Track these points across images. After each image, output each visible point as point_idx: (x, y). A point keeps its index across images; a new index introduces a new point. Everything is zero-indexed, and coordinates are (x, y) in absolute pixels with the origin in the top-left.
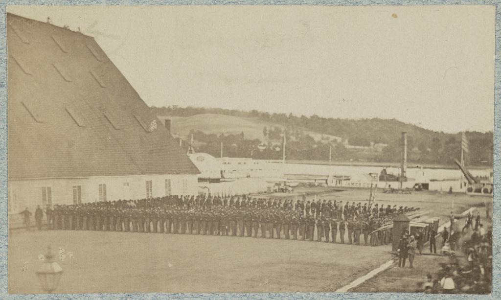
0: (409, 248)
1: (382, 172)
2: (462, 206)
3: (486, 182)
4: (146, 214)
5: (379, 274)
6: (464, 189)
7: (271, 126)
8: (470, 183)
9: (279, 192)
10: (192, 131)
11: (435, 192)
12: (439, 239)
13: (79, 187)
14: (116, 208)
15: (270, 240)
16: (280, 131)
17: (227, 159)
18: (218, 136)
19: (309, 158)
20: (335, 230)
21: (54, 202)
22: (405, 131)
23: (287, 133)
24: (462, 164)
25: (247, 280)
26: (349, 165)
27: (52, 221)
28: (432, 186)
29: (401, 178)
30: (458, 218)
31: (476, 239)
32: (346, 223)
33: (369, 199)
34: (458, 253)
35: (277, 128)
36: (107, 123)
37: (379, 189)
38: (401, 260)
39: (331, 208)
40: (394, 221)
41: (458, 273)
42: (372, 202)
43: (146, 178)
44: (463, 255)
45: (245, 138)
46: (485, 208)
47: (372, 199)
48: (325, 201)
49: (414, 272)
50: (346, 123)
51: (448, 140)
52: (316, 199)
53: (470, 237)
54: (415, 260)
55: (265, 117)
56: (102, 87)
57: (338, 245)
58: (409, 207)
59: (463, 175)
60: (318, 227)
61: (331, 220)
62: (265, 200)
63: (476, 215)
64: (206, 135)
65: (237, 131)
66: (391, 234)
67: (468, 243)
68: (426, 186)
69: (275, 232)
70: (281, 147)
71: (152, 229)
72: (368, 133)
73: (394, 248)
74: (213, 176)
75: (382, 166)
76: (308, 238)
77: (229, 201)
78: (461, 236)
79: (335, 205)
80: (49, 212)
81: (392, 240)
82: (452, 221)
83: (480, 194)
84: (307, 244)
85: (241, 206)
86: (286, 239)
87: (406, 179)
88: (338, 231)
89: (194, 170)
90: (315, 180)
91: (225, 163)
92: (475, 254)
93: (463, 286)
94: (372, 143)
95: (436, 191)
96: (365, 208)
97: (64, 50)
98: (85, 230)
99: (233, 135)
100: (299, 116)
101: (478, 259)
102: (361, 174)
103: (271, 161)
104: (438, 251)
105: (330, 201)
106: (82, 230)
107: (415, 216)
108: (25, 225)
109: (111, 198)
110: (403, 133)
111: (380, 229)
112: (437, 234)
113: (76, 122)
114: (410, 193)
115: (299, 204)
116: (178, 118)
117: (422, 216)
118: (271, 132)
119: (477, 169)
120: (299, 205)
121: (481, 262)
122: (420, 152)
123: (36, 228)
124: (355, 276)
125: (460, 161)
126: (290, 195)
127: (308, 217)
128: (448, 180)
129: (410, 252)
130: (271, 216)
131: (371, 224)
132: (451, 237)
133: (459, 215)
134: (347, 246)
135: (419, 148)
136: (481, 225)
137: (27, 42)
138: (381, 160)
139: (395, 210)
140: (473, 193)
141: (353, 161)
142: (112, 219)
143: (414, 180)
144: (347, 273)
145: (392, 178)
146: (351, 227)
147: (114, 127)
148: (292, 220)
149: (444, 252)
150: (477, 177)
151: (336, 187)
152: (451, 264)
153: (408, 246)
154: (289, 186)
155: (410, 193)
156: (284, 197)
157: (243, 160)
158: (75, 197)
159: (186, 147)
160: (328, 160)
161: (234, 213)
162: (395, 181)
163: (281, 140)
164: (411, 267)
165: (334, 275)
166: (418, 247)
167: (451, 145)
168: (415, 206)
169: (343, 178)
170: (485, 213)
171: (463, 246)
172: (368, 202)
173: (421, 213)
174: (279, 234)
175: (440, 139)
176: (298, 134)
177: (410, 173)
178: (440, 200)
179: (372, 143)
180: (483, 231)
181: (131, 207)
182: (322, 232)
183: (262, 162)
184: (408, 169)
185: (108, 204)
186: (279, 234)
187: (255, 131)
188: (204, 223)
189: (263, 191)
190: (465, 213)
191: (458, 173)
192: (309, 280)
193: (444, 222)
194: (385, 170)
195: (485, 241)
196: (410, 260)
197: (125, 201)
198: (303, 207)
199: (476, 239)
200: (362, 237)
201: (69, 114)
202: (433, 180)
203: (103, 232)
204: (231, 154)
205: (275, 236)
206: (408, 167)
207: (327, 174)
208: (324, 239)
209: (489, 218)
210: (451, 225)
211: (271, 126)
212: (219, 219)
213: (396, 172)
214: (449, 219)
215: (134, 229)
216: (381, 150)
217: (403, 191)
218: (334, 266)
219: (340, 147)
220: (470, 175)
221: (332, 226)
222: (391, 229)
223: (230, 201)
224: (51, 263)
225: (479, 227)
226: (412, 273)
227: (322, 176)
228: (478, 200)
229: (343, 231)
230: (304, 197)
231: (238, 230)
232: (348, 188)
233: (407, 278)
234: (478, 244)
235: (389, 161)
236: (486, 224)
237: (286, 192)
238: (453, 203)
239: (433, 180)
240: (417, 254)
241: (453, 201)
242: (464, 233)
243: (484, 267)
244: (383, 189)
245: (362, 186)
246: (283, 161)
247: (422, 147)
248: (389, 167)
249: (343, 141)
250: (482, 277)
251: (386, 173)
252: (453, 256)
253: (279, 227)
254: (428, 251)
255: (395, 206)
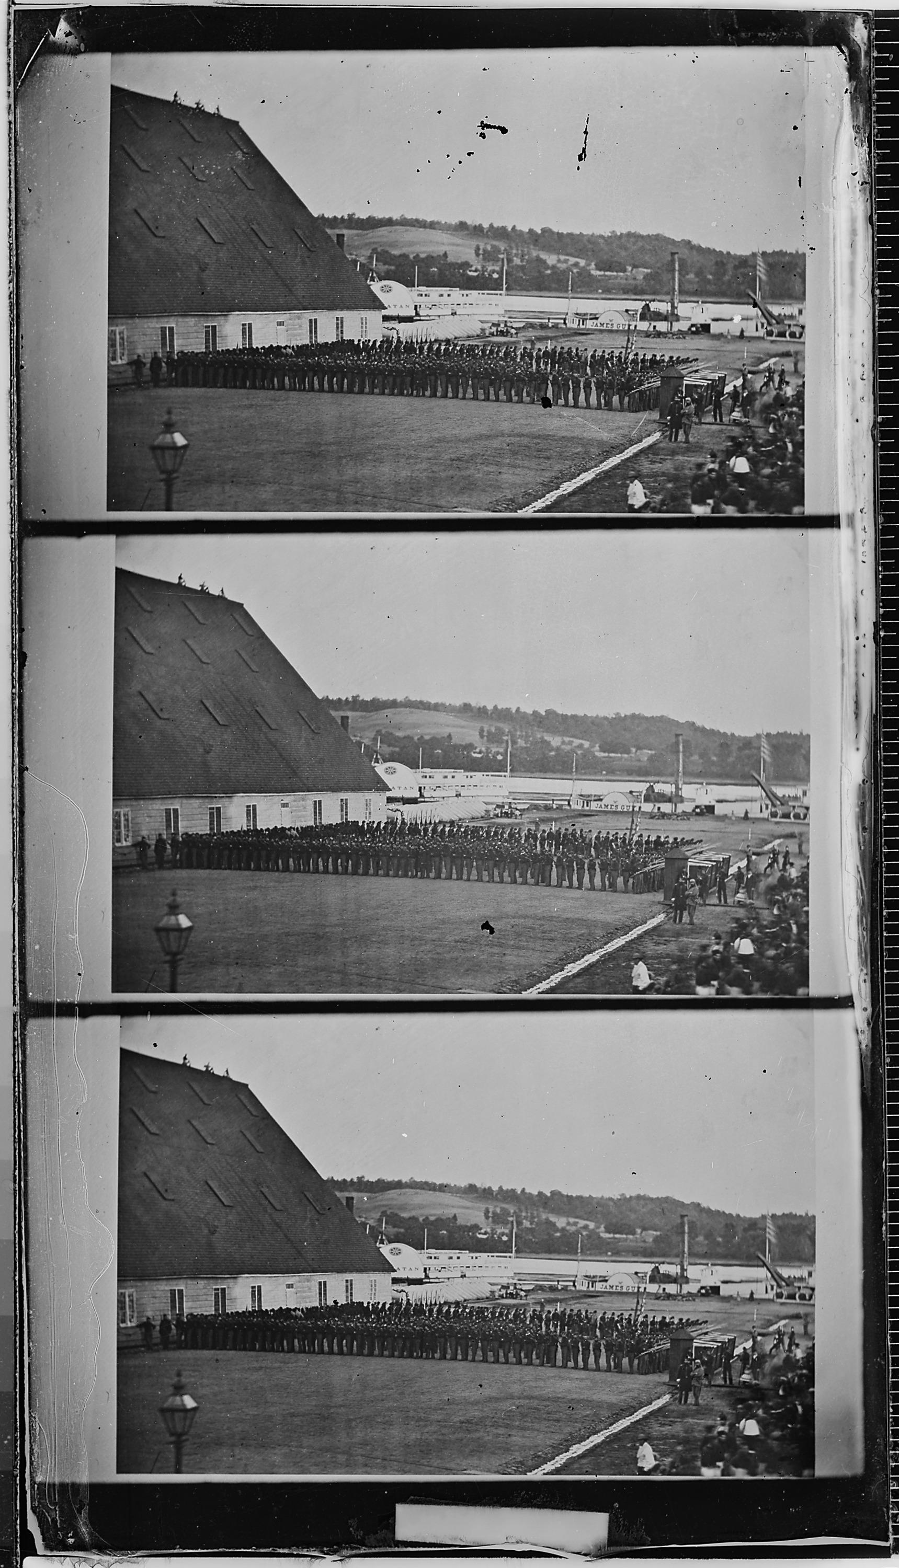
0: (688, 896)
1: (653, 1271)
2: (763, 837)
3: (802, 1285)
4: (313, 846)
5: (641, 451)
6: (771, 1295)
7: (495, 1207)
8: (774, 805)
9: (497, 335)
10: (379, 732)
11: (729, 1299)
12: (731, 883)
13: (218, 809)
14: (275, 1319)
15: (484, 403)
16: (503, 734)
17: (423, 289)
18: (411, 257)
19: (540, 289)
20: (581, 871)
21: (181, 830)
22: (685, 1213)
23: (518, 1217)
24: (768, 1260)
25: (456, 942)
26: (601, 780)
27: (183, 1337)
28: (719, 809)
29: (671, 317)
30: (758, 854)
31: (784, 883)
32: (598, 861)
33: (634, 1307)
34: (758, 903)
35: (497, 729)
36: (260, 721)
37: (640, 332)
38: (676, 913)
39: (576, 841)
40: (666, 858)
41: (764, 1413)
42: (633, 832)
43: (310, 315)
44: (765, 906)
45: (453, 742)
46: (796, 840)
47: (630, 346)
48: (562, 348)
49: (691, 449)
50: (592, 240)
51: (737, 263)
52: (550, 346)
53: (775, 882)
54: (692, 431)
55: (477, 231)
56: (249, 189)
57: (591, 1373)
58: (688, 838)
59: (769, 1275)
60: (562, 1348)
61: (572, 375)
62: (487, 1309)
63: (789, 1330)
64: (395, 256)
65: (439, 250)
66: (662, 876)
67: (771, 889)
68: (710, 809)
69: (492, 391)
70: (500, 273)
71: (316, 386)
72: (623, 253)
73: (672, 1378)
74: (413, 1276)
75: (642, 300)
76: (543, 882)
77: (426, 347)
78: (762, 878)
79: (581, 836)
80: (170, 362)
81: (663, 885)
82: (749, 858)
83: (784, 339)
84: (549, 1372)
85: (453, 1318)
86: (516, 1364)
87: (687, 1281)
88: (592, 1352)
89: (381, 786)
90: (549, 319)
91: (422, 295)
92: (783, 905)
93: (768, 950)
94: (634, 750)
95: (721, 335)
96: (629, 1320)
97: (202, 621)
98: (225, 869)
99: (442, 1220)
100: (530, 711)
101: (783, 430)
102: (612, 311)
103: (486, 292)
104: (725, 419)
105: (570, 348)
106: (221, 869)
107: (695, 851)
108: (145, 1343)
109: (268, 1305)
110: (682, 1217)
111: (652, 1350)
112: (733, 1357)
113: (216, 719)
114: (689, 819)
115: (530, 833)
116: (358, 714)
117: (701, 370)
118: (494, 1213)
119: (784, 785)
120: (531, 836)
121: (792, 916)
122: (697, 280)
123: (156, 866)
124: (611, 936)
125: (760, 775)
126: (517, 821)
127: (542, 853)
128: (746, 1282)
129: (684, 420)
130: (495, 1331)
131: (632, 862)
132: (746, 881)
133: (759, 850)
134: (594, 412)
135: (697, 275)
136: (797, 1345)
137: (149, 609)
138: (652, 1255)
139: (663, 361)
140: (783, 1300)
141: (611, 1256)
142: (259, 371)
143: (699, 1281)
144: (594, 450)
145: (668, 1279)
146: (609, 1348)
147: (274, 1207)
148: (525, 1337)
149: (735, 420)
150: (789, 1277)
151: (587, 1291)
152: (749, 919)
153: (687, 893)
154: (512, 328)
155: (689, 819)
156: (509, 824)
157: (449, 772)
158: (212, 823)
159: (376, 1234)
160: (567, 291)
161: (438, 846)
162: (666, 802)
163: (504, 745)
164: (687, 441)
165: (582, 935)
166: (696, 414)
167: (752, 1233)
168: (691, 355)
169: (598, 1279)
170: (793, 365)
171: (766, 893)
172: (633, 1313)
173: (705, 847)
174: (501, 877)
175: (725, 261)
176: (527, 736)
177: (693, 1272)
178: (730, 347)
179: (639, 1231)
180: (789, 391)
181: (291, 836)
182: (563, 875)
183: (474, 293)
184: (690, 1267)
185: (254, 351)
186: (501, 877)
187: (463, 251)
188: (391, 380)
189: (475, 334)
190: (763, 366)
191: (762, 1273)
192: (542, 460)
193: (737, 860)
194: (647, 305)
195: (796, 887)
196: (685, 432)
197: (279, 347)
198: (535, 839)
199: (784, 883)
200: (616, 399)
201: (207, 708)
202: (724, 1282)
203: (246, 391)
204: (439, 1244)
205: (492, 397)
206: (690, 1264)
207: (575, 1274)
208: (571, 1364)
209: (797, 372)
210: (754, 1345)
211: (490, 725)
212: (416, 854)
213: (674, 1270)
214: (740, 374)
215: (300, 1347)
216: (651, 1240)
217: (683, 1297)
218: (588, 1403)
219: (593, 1235)
220: (778, 1274)
221: (582, 1345)
222: (662, 869)
223: (428, 348)
224: (182, 1395)
225: (788, 867)
226: (692, 931)
227: (562, 795)
228: (788, 830)
229: (592, 872)
230: (537, 824)
231: (440, 389)
232: (600, 811)
233: (681, 458)
234: (792, 1372)
235: (664, 1256)
236: (804, 1343)
237: (506, 336)
238: (755, 1313)
239: (724, 1282)
240: (696, 424)
241: (755, 1313)
242: (772, 1356)
243: (796, 923)
244: (655, 1294)
245: (615, 328)
246: (503, 292)
247: (709, 1236)
248: (663, 1263)
249: (598, 1228)
250: (794, 937)
251: (659, 1272)
252: (746, 426)
253: (507, 1347)
254: (712, 420)
255: (668, 837)
